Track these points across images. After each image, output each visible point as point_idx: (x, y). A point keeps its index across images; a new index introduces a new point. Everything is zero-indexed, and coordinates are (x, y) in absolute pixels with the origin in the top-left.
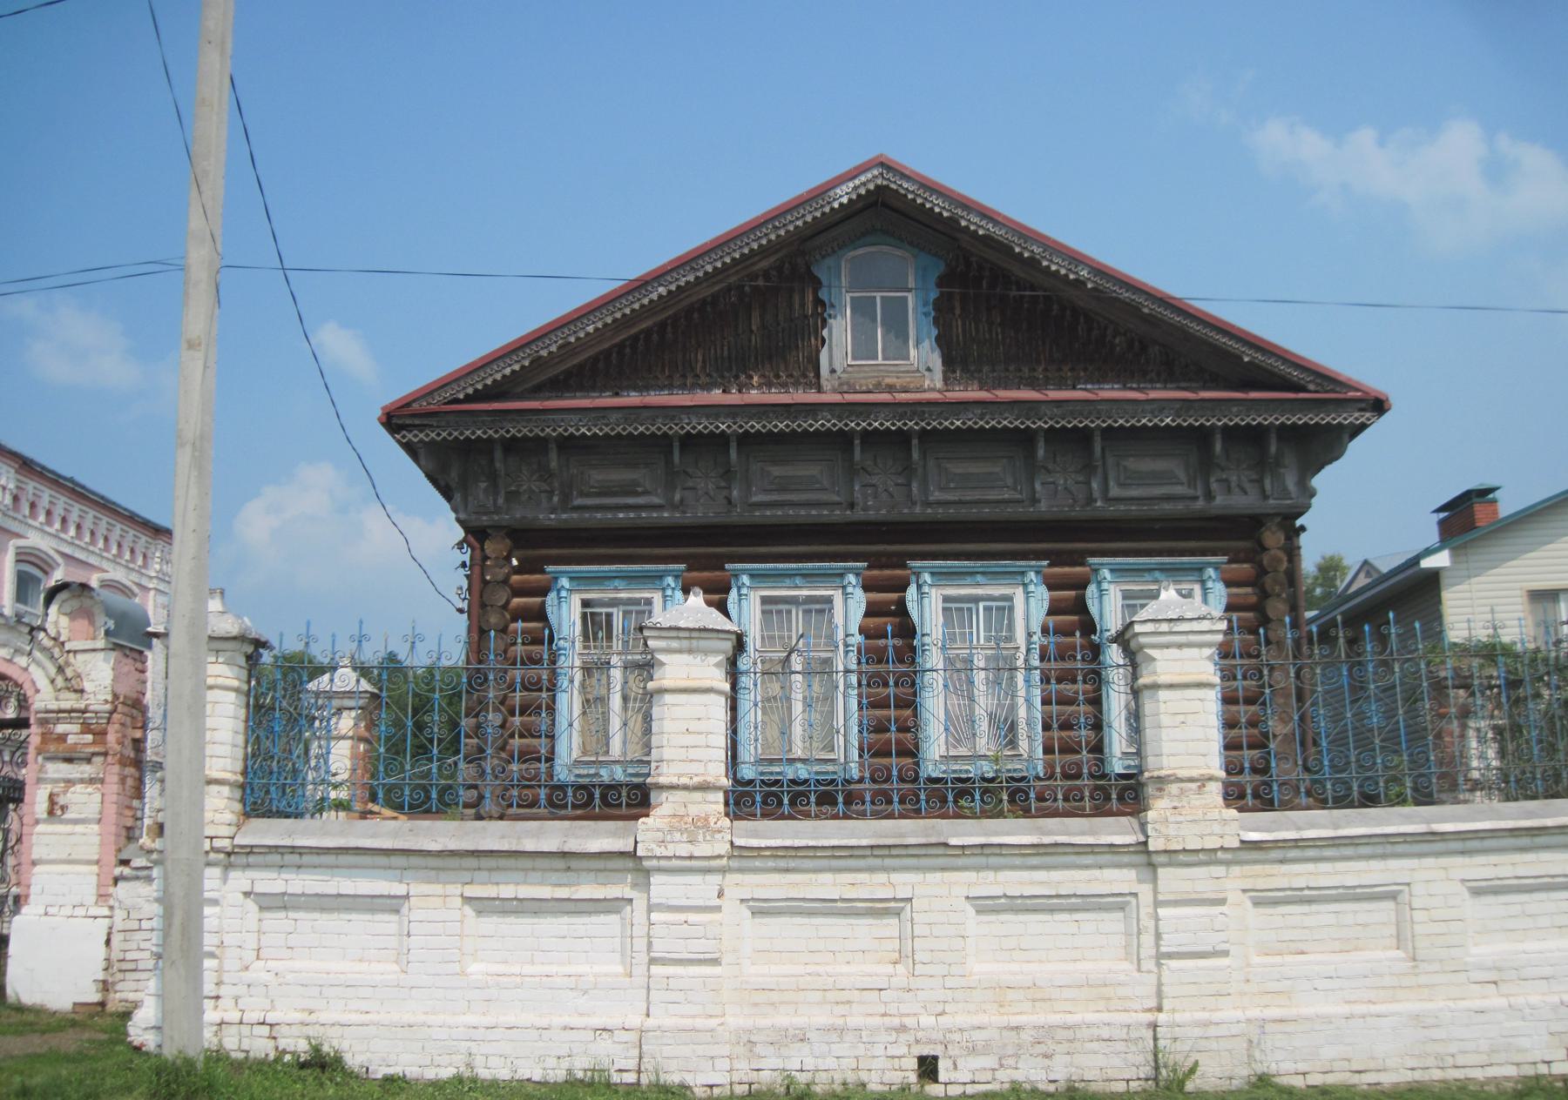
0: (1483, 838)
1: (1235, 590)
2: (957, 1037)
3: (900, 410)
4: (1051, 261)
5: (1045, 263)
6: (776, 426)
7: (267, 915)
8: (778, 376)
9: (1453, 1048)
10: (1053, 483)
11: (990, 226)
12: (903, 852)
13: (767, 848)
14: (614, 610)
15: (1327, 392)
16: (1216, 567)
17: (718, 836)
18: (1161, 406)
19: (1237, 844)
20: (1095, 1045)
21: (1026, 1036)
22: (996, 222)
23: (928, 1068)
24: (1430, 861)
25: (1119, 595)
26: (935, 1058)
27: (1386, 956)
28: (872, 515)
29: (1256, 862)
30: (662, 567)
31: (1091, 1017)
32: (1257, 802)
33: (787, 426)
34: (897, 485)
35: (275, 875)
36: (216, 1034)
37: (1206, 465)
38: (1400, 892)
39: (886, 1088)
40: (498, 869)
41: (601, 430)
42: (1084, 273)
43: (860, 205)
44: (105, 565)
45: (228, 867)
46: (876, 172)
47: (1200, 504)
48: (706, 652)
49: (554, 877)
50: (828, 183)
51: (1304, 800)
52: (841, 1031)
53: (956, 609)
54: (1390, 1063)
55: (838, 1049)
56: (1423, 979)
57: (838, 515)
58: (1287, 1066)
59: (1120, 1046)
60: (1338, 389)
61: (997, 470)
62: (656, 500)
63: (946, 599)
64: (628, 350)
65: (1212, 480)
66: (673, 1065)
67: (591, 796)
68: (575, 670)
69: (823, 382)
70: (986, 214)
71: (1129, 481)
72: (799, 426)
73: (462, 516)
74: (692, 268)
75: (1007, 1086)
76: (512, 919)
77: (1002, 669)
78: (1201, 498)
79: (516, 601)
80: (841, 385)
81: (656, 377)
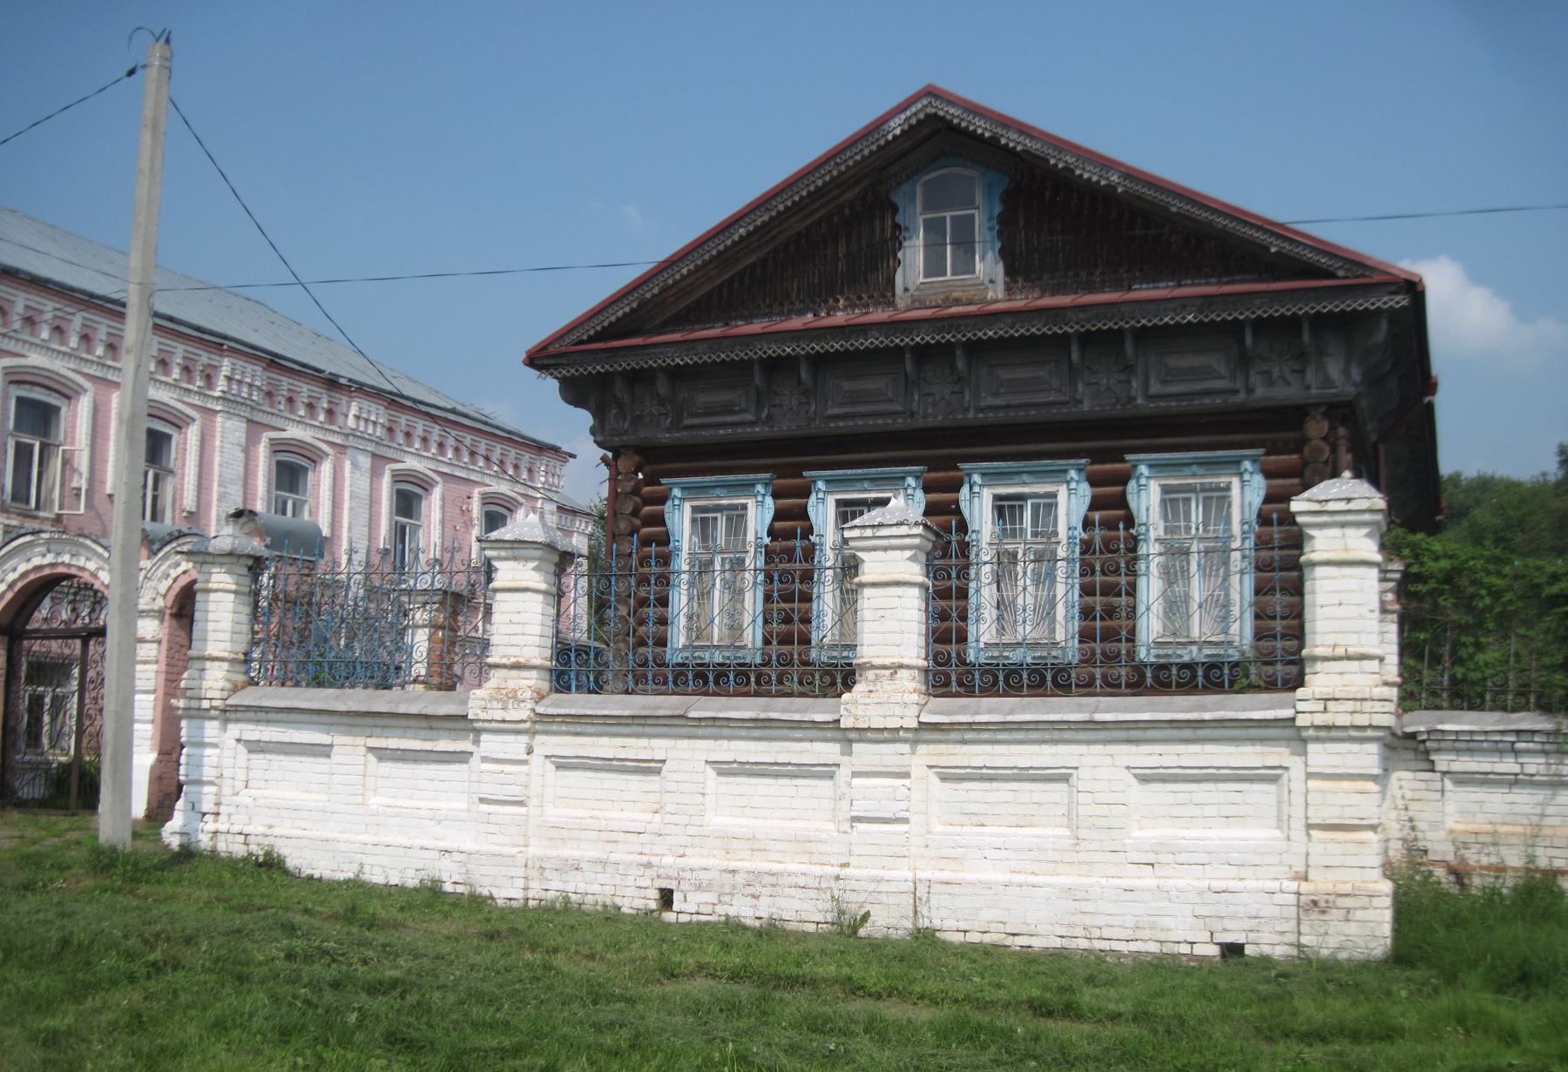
0: (1146, 729)
2: (687, 875)
3: (939, 325)
4: (1084, 169)
5: (1078, 172)
6: (832, 347)
7: (253, 756)
8: (860, 298)
9: (1101, 921)
10: (1097, 383)
11: (1027, 141)
12: (655, 722)
13: (558, 716)
14: (719, 515)
15: (1356, 277)
16: (1254, 460)
17: (522, 705)
18: (1183, 303)
19: (915, 725)
20: (793, 891)
22: (1032, 137)
23: (666, 898)
25: (1158, 489)
26: (671, 891)
27: (1054, 833)
28: (930, 422)
29: (940, 742)
30: (752, 476)
31: (792, 867)
32: (961, 690)
33: (842, 346)
34: (1119, 382)
35: (253, 727)
36: (212, 839)
37: (1243, 362)
38: (1071, 775)
39: (634, 912)
40: (356, 726)
41: (737, 355)
42: (1115, 178)
43: (926, 131)
44: (487, 480)
45: (227, 721)
46: (925, 102)
47: (1241, 397)
48: (526, 559)
49: (423, 733)
50: (882, 117)
51: (651, 686)
52: (604, 863)
53: (1009, 506)
54: (1040, 930)
55: (602, 878)
56: (1083, 856)
57: (900, 423)
58: (949, 924)
59: (812, 893)
60: (1367, 273)
61: (1042, 374)
62: (749, 417)
63: (997, 498)
64: (736, 284)
65: (1252, 372)
66: (486, 881)
67: (1043, 678)
68: (752, 567)
69: (898, 300)
70: (1024, 130)
71: (1169, 378)
72: (852, 345)
73: (600, 439)
74: (767, 209)
75: (723, 918)
76: (400, 765)
77: (1218, 554)
78: (1243, 391)
79: (647, 509)
80: (913, 302)
81: (759, 307)
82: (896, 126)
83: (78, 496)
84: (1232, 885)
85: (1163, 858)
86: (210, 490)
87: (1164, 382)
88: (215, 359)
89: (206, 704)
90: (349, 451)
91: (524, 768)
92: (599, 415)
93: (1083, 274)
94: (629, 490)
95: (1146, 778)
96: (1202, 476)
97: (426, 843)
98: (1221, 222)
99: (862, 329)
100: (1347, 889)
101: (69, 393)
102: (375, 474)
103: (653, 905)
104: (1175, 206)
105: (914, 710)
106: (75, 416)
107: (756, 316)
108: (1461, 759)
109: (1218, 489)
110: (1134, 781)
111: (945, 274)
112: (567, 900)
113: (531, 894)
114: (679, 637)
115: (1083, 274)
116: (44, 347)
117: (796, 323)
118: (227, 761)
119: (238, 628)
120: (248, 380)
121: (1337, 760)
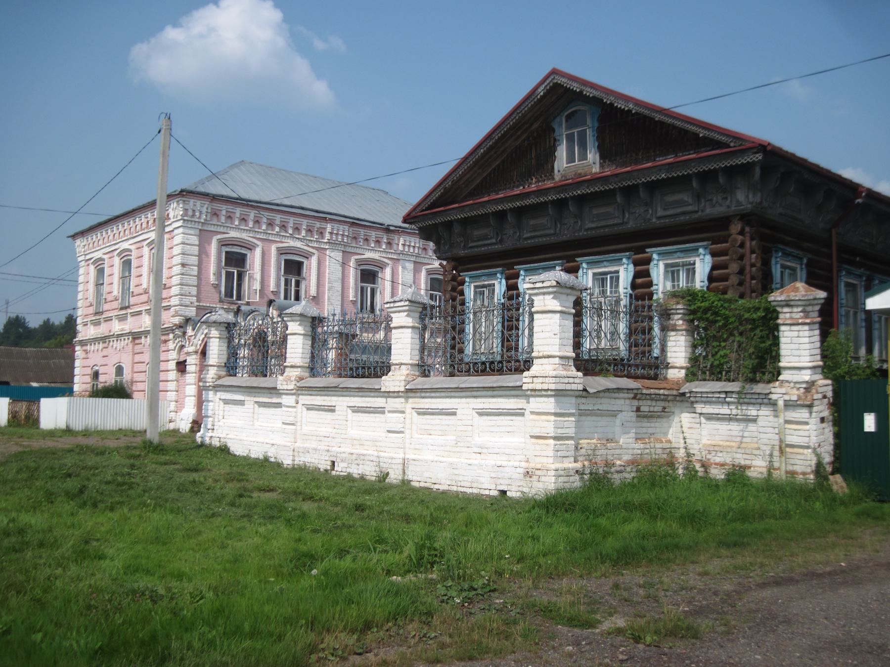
1: (716, 259)
5: (615, 105)
7: (225, 406)
8: (541, 177)
14: (485, 289)
16: (705, 248)
21: (354, 457)
22: (596, 89)
23: (333, 463)
24: (464, 400)
28: (564, 238)
30: (494, 270)
42: (631, 106)
45: (217, 391)
54: (443, 481)
55: (315, 456)
56: (458, 449)
57: (553, 239)
58: (415, 478)
62: (494, 241)
82: (541, 91)
83: (256, 293)
84: (504, 463)
85: (484, 451)
86: (324, 285)
87: (665, 209)
88: (323, 225)
89: (208, 384)
90: (401, 262)
91: (294, 410)
92: (437, 243)
93: (634, 155)
94: (449, 279)
95: (482, 413)
96: (683, 258)
97: (268, 441)
98: (678, 123)
99: (527, 195)
100: (539, 466)
101: (251, 248)
102: (416, 271)
103: (329, 468)
104: (658, 117)
105: (403, 383)
106: (254, 257)
107: (500, 190)
108: (707, 406)
109: (690, 264)
110: (477, 415)
111: (575, 162)
112: (305, 466)
113: (295, 463)
114: (469, 349)
115: (634, 155)
116: (237, 228)
117: (517, 192)
118: (217, 408)
119: (222, 353)
120: (341, 233)
121: (540, 406)
